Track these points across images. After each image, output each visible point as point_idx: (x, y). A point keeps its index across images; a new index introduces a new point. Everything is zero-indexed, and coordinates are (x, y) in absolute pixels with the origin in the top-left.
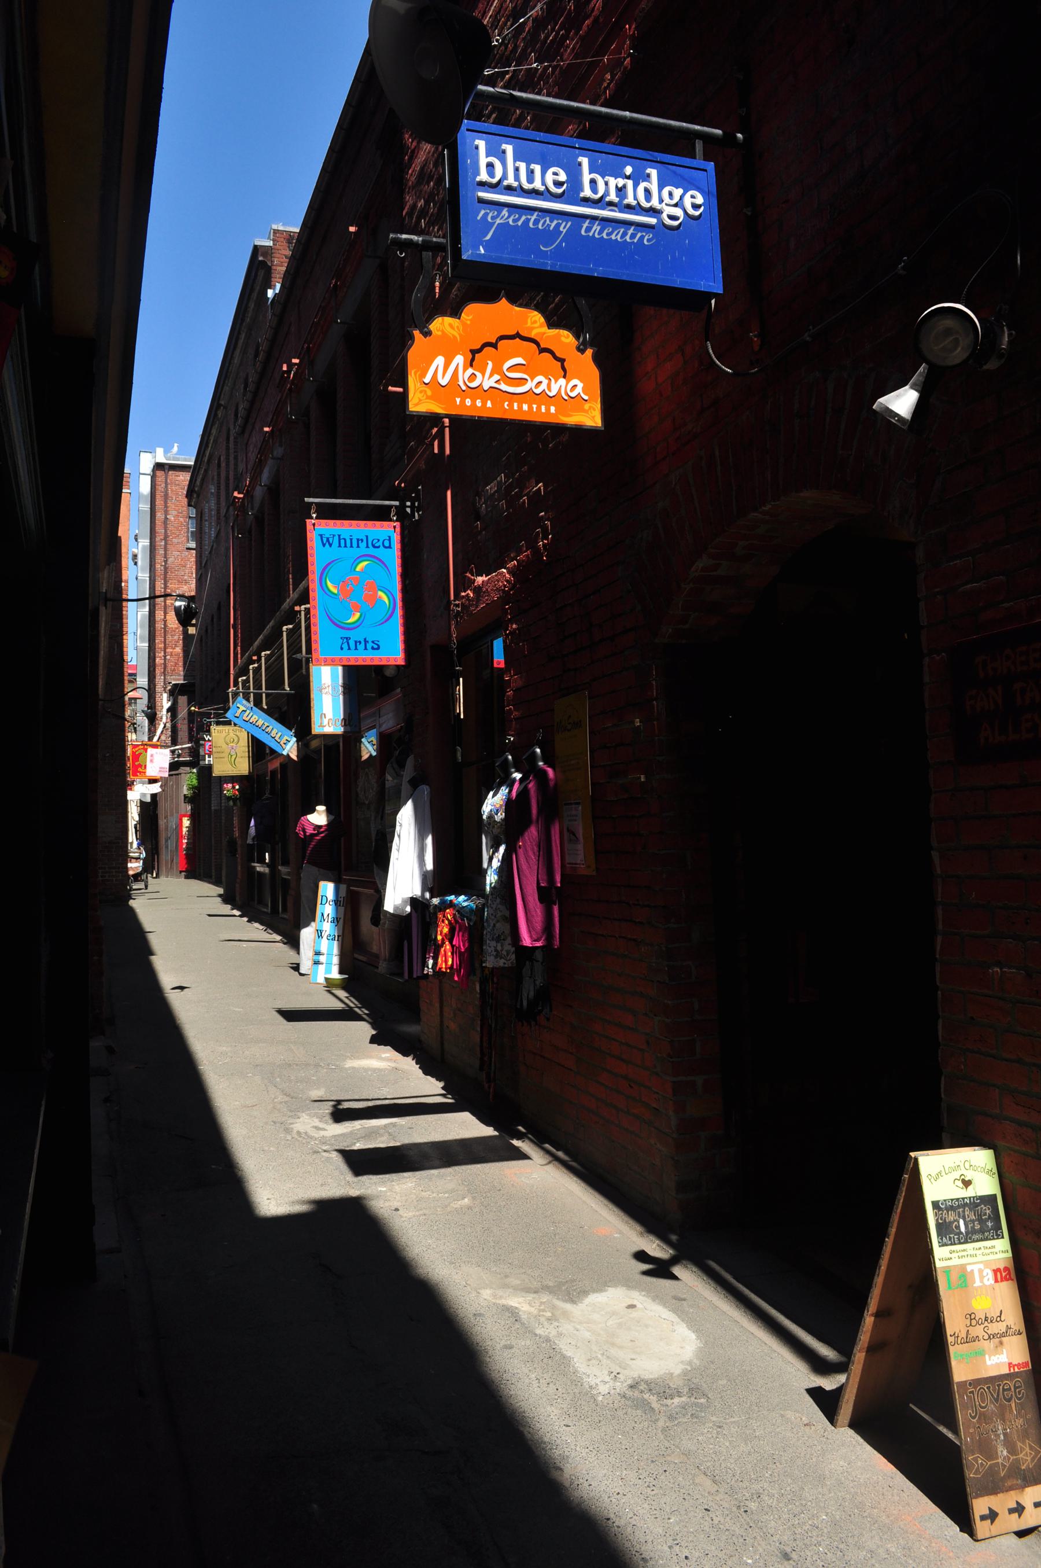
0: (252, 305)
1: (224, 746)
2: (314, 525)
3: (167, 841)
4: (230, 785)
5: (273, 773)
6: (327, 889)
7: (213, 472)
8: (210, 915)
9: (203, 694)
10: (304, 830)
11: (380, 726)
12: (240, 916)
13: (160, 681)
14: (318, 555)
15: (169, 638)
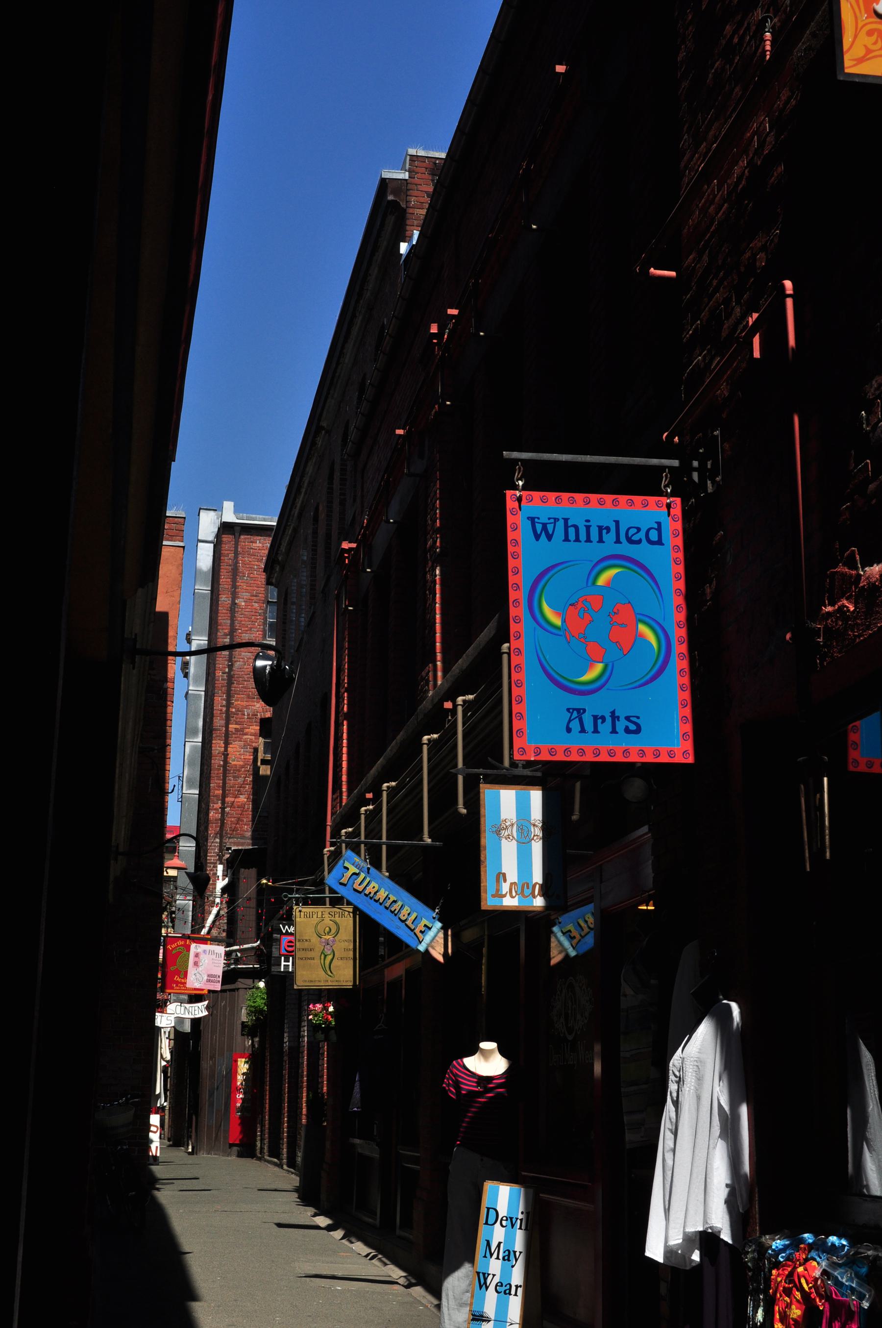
0: (375, 271)
1: (315, 939)
2: (519, 500)
3: (211, 1095)
4: (319, 1006)
5: (394, 985)
8: (280, 1225)
9: (283, 857)
10: (457, 1085)
12: (329, 1228)
13: (214, 844)
14: (526, 555)
15: (231, 781)
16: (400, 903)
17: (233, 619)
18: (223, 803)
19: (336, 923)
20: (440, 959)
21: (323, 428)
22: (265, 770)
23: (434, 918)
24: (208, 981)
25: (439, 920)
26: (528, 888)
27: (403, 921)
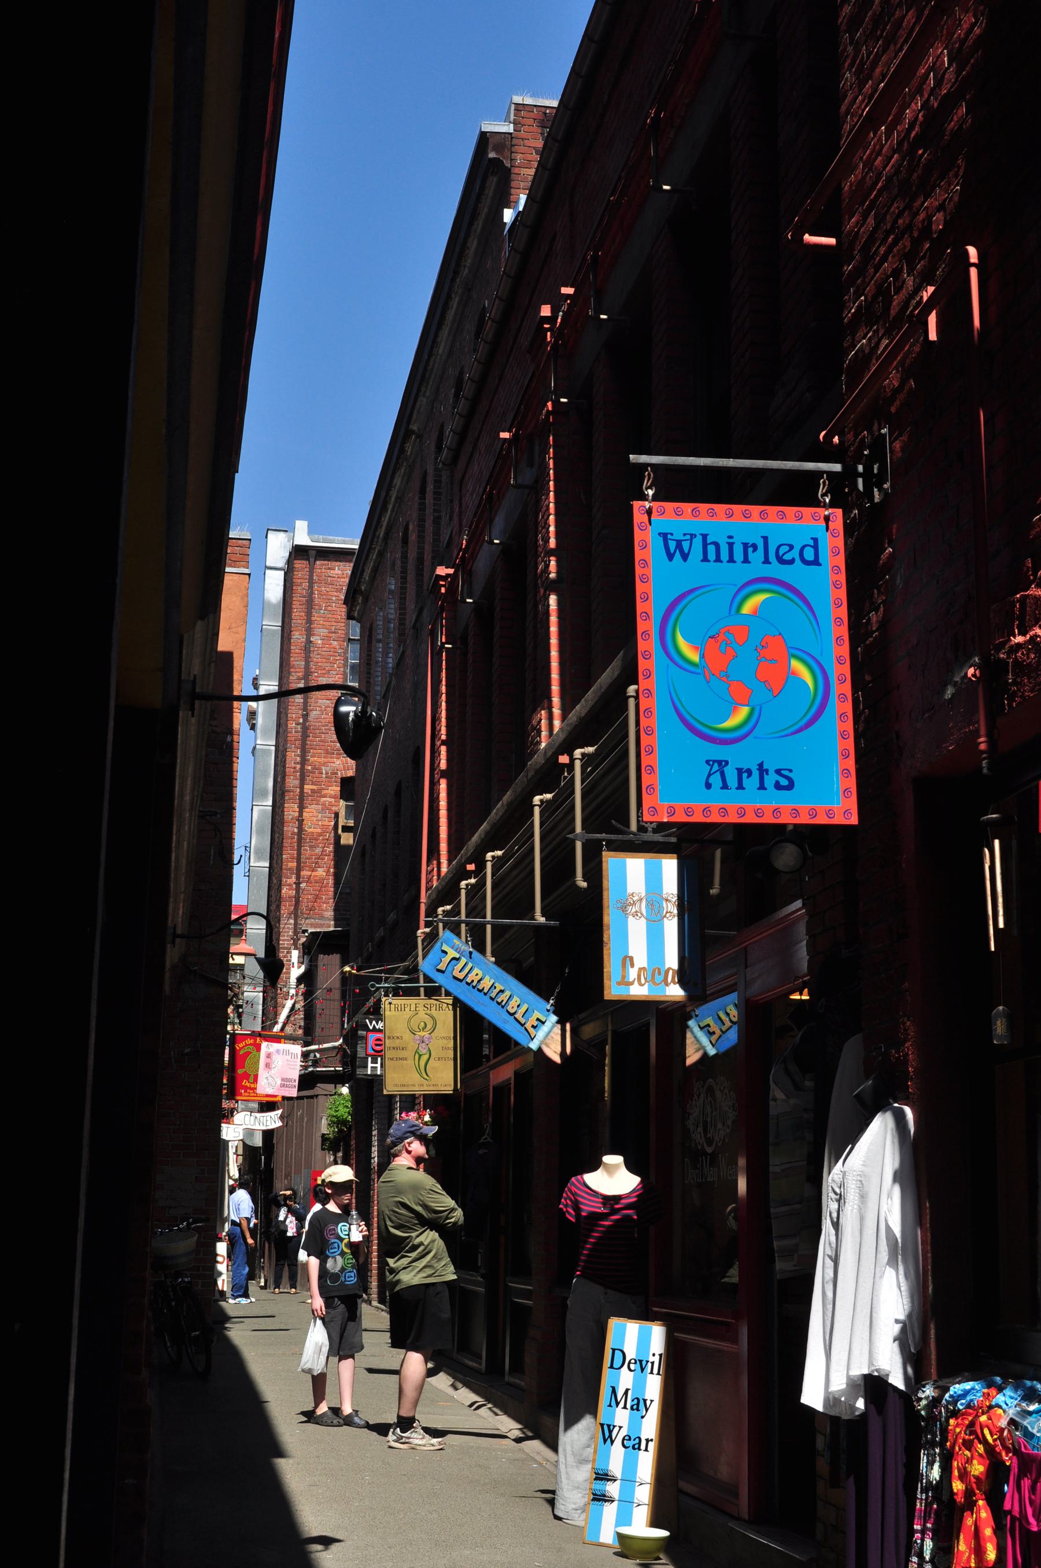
0: (473, 244)
1: (407, 1036)
2: (649, 512)
5: (501, 1090)
6: (637, 1342)
7: (394, 554)
8: (371, 1371)
9: (373, 936)
11: (747, 985)
14: (657, 579)
15: (306, 851)
16: (507, 993)
17: (307, 659)
18: (298, 877)
19: (432, 1017)
20: (557, 1059)
21: (413, 432)
22: (347, 839)
23: (548, 1011)
24: (282, 1086)
25: (555, 1013)
26: (659, 973)
27: (512, 1014)
